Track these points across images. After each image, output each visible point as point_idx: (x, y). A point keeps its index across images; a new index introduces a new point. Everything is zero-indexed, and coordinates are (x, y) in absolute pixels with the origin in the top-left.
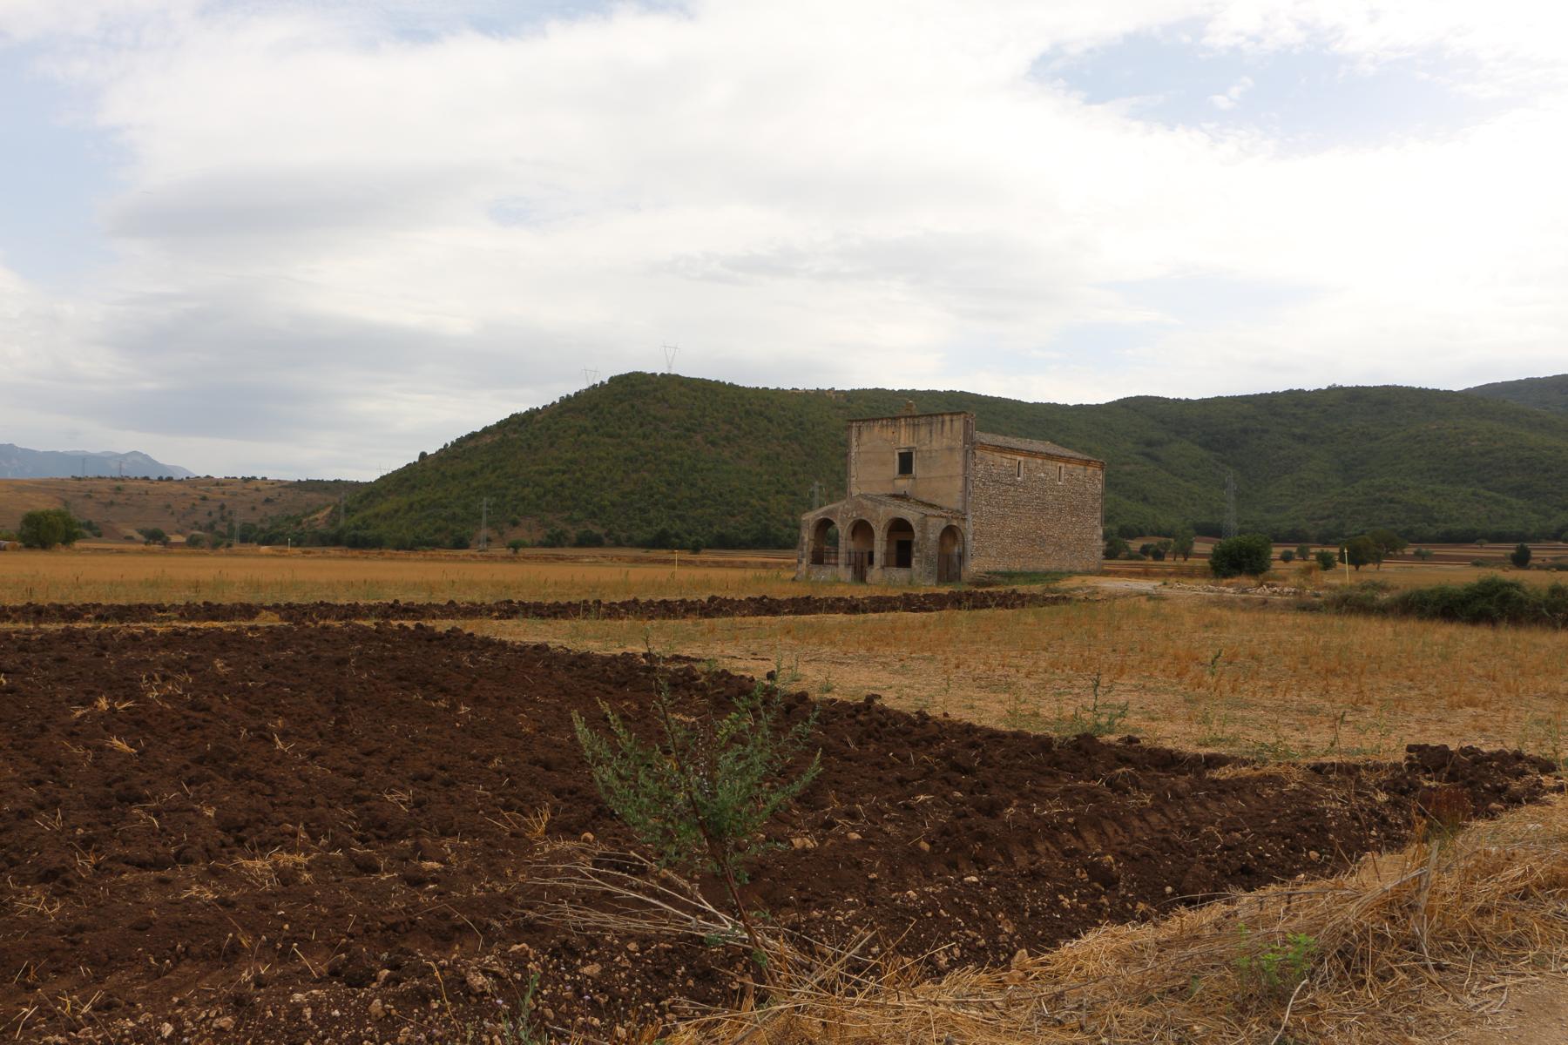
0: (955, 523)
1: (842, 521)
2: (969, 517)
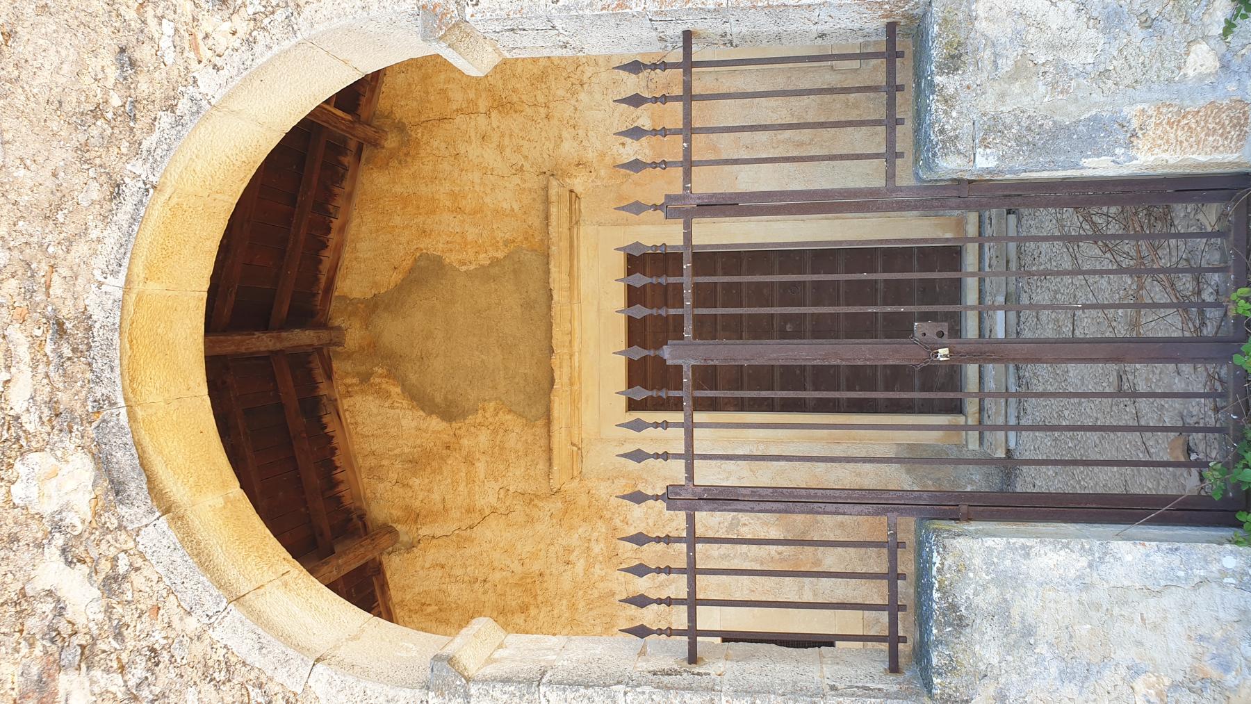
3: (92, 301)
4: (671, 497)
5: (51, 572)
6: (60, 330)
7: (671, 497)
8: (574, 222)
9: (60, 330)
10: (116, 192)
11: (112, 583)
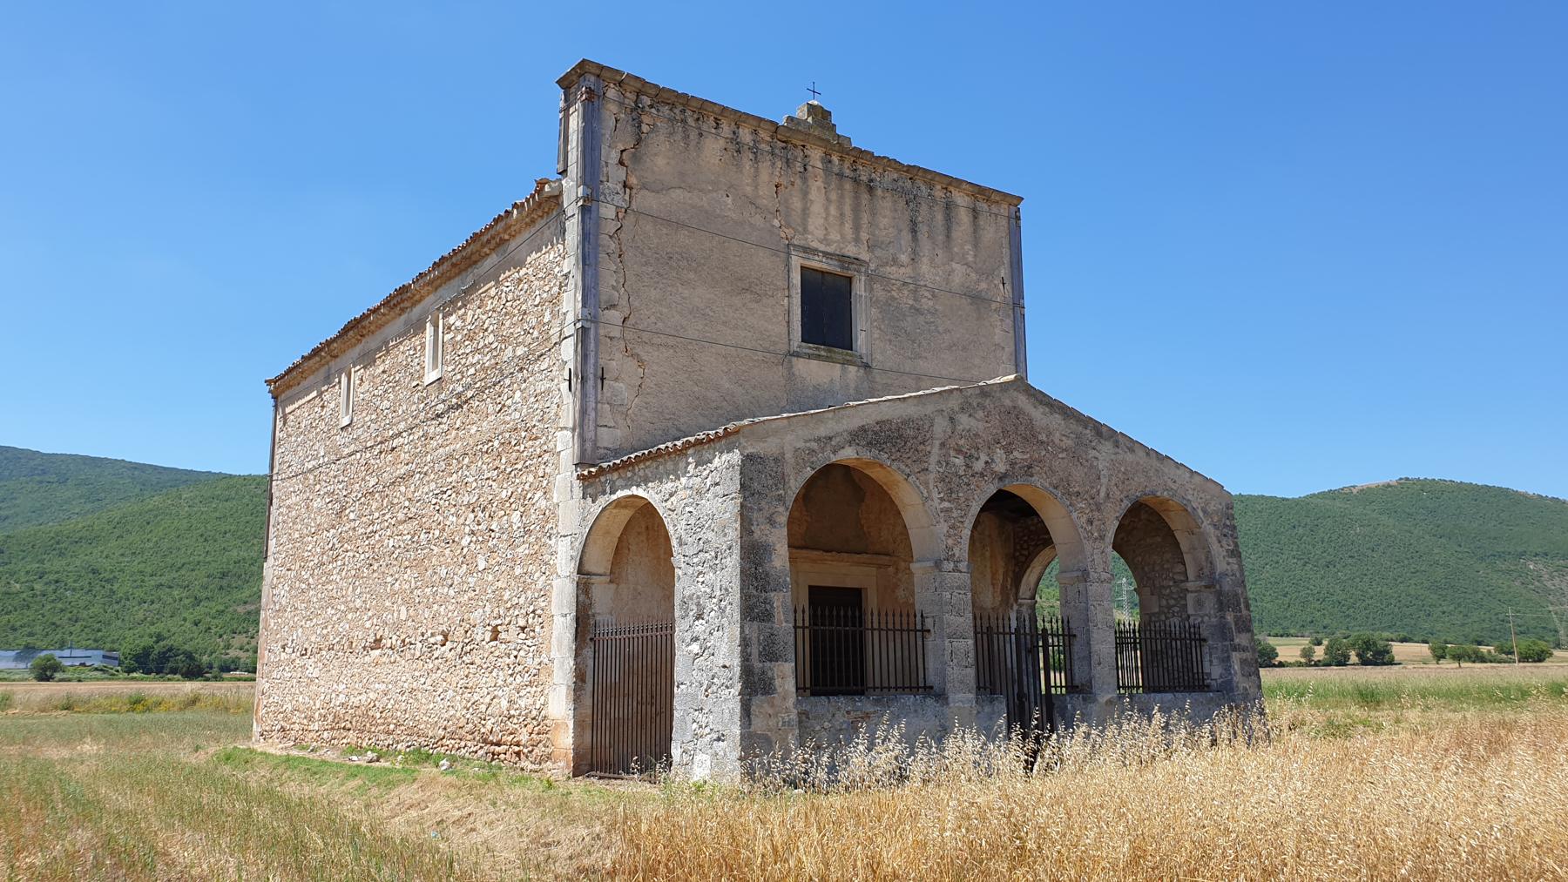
5: (984, 458)
8: (880, 566)
9: (1030, 467)
11: (982, 475)
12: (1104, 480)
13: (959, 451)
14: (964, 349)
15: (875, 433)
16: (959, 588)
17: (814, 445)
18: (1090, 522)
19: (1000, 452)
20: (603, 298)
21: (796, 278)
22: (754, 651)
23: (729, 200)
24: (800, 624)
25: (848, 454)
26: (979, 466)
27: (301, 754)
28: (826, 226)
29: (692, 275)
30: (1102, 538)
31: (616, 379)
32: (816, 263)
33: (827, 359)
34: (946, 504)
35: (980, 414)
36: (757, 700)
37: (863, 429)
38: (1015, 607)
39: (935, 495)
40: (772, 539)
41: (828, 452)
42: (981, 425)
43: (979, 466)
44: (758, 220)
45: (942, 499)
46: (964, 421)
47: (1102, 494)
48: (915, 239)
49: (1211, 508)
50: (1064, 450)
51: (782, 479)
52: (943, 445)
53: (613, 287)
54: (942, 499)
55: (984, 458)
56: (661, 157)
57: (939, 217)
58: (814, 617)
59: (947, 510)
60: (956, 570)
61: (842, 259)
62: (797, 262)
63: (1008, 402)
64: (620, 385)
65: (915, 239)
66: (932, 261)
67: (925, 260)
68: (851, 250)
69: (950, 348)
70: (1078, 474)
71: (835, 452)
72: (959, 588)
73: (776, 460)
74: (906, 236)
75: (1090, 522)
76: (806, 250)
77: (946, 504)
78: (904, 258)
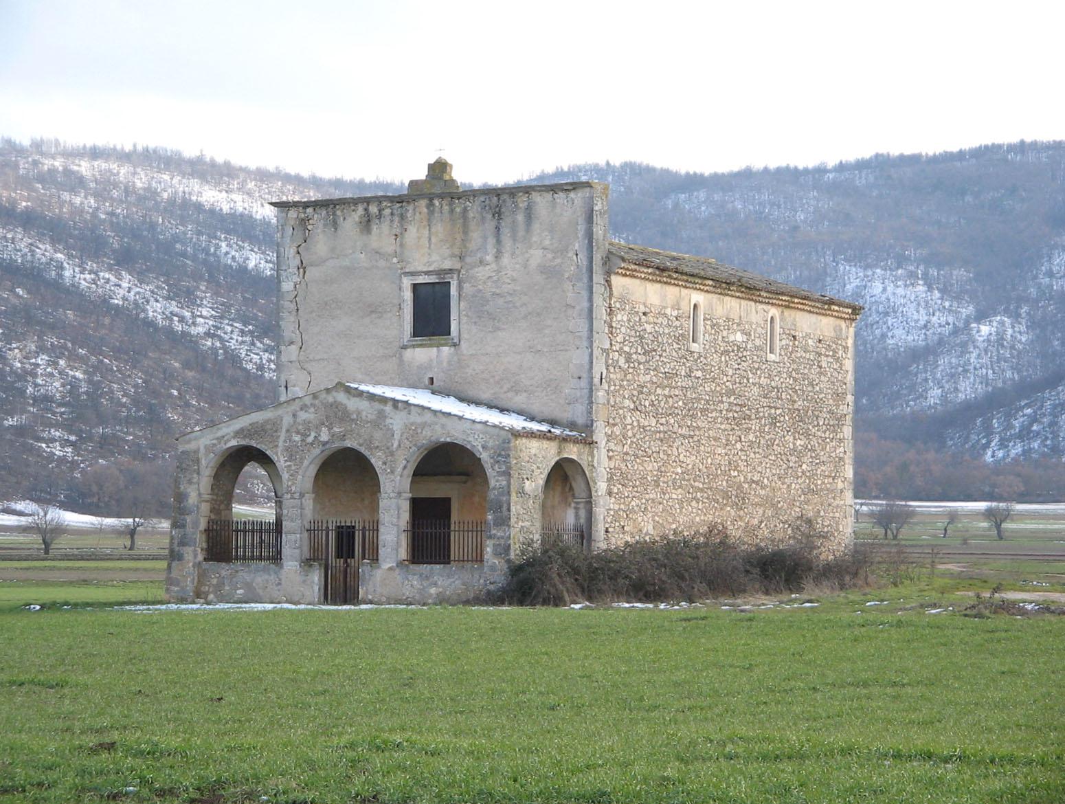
0: (572, 452)
1: (291, 453)
2: (600, 435)
3: (347, 441)
4: (364, 528)
5: (313, 434)
6: (344, 436)
7: (328, 528)
9: (344, 436)
10: (360, 446)
11: (312, 444)
12: (397, 437)
13: (298, 432)
14: (539, 315)
15: (249, 430)
16: (293, 507)
17: (215, 442)
18: (385, 463)
19: (324, 429)
20: (286, 339)
21: (408, 295)
22: (176, 542)
23: (363, 256)
24: (375, 533)
25: (234, 443)
26: (310, 439)
27: (156, 607)
28: (425, 250)
29: (338, 312)
30: (392, 472)
31: (294, 386)
32: (421, 280)
33: (431, 346)
34: (289, 463)
35: (312, 410)
36: (174, 564)
37: (242, 430)
38: (573, 505)
39: (282, 459)
40: (189, 490)
41: (222, 444)
42: (312, 416)
43: (310, 439)
44: (382, 263)
45: (286, 461)
46: (303, 416)
47: (395, 445)
48: (499, 242)
49: (490, 444)
50: (368, 422)
51: (198, 461)
52: (288, 431)
53: (293, 332)
54: (286, 461)
55: (313, 434)
56: (321, 243)
57: (520, 218)
58: (413, 525)
59: (290, 466)
60: (292, 498)
61: (439, 272)
62: (407, 283)
63: (331, 400)
64: (297, 389)
65: (499, 242)
66: (513, 254)
67: (506, 255)
68: (447, 265)
69: (525, 317)
70: (378, 435)
71: (225, 444)
72: (293, 507)
73: (195, 452)
74: (491, 241)
75: (385, 463)
76: (413, 274)
77: (289, 463)
78: (489, 258)
